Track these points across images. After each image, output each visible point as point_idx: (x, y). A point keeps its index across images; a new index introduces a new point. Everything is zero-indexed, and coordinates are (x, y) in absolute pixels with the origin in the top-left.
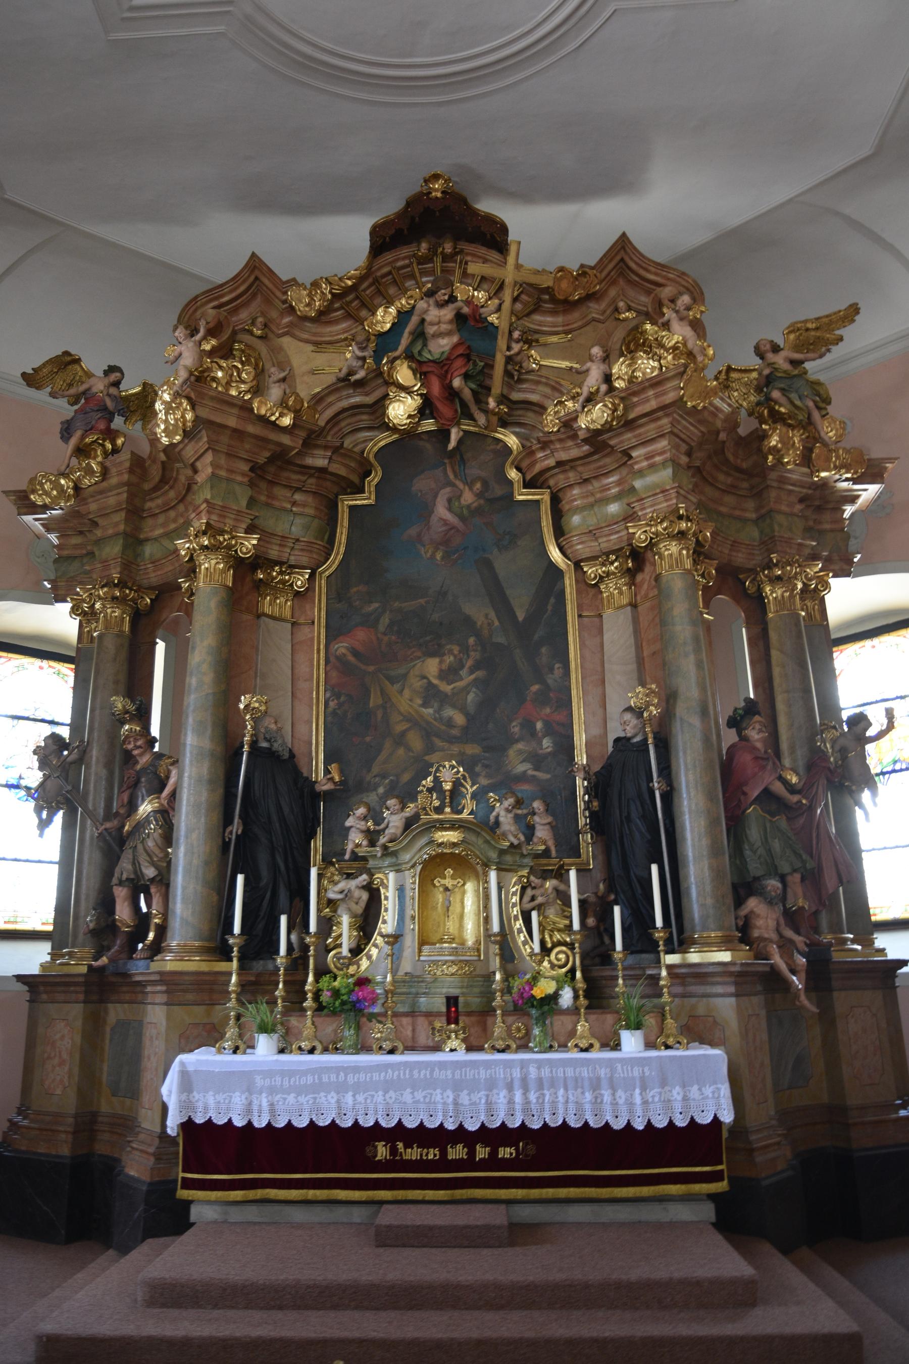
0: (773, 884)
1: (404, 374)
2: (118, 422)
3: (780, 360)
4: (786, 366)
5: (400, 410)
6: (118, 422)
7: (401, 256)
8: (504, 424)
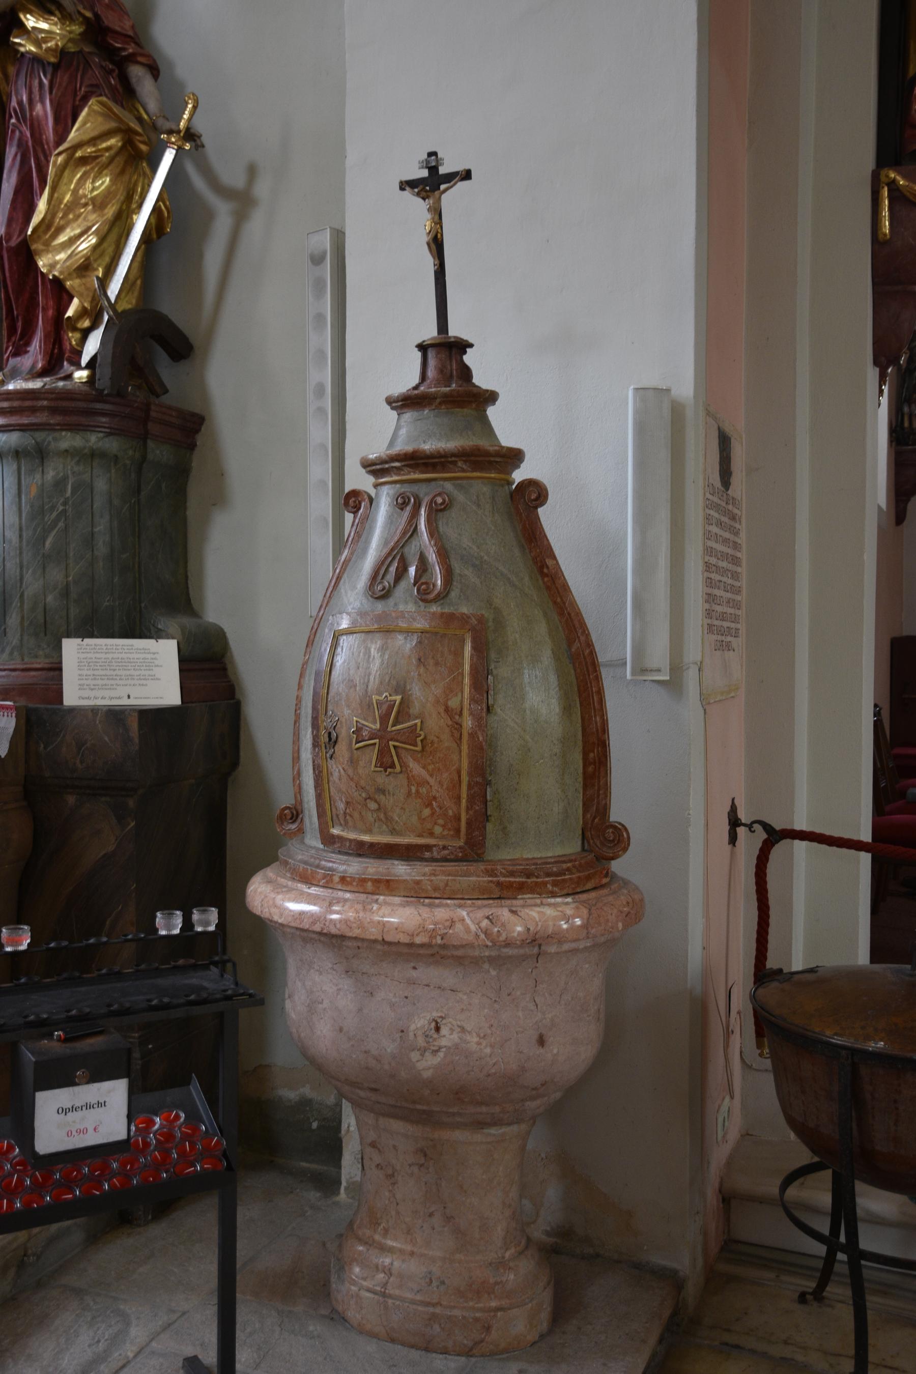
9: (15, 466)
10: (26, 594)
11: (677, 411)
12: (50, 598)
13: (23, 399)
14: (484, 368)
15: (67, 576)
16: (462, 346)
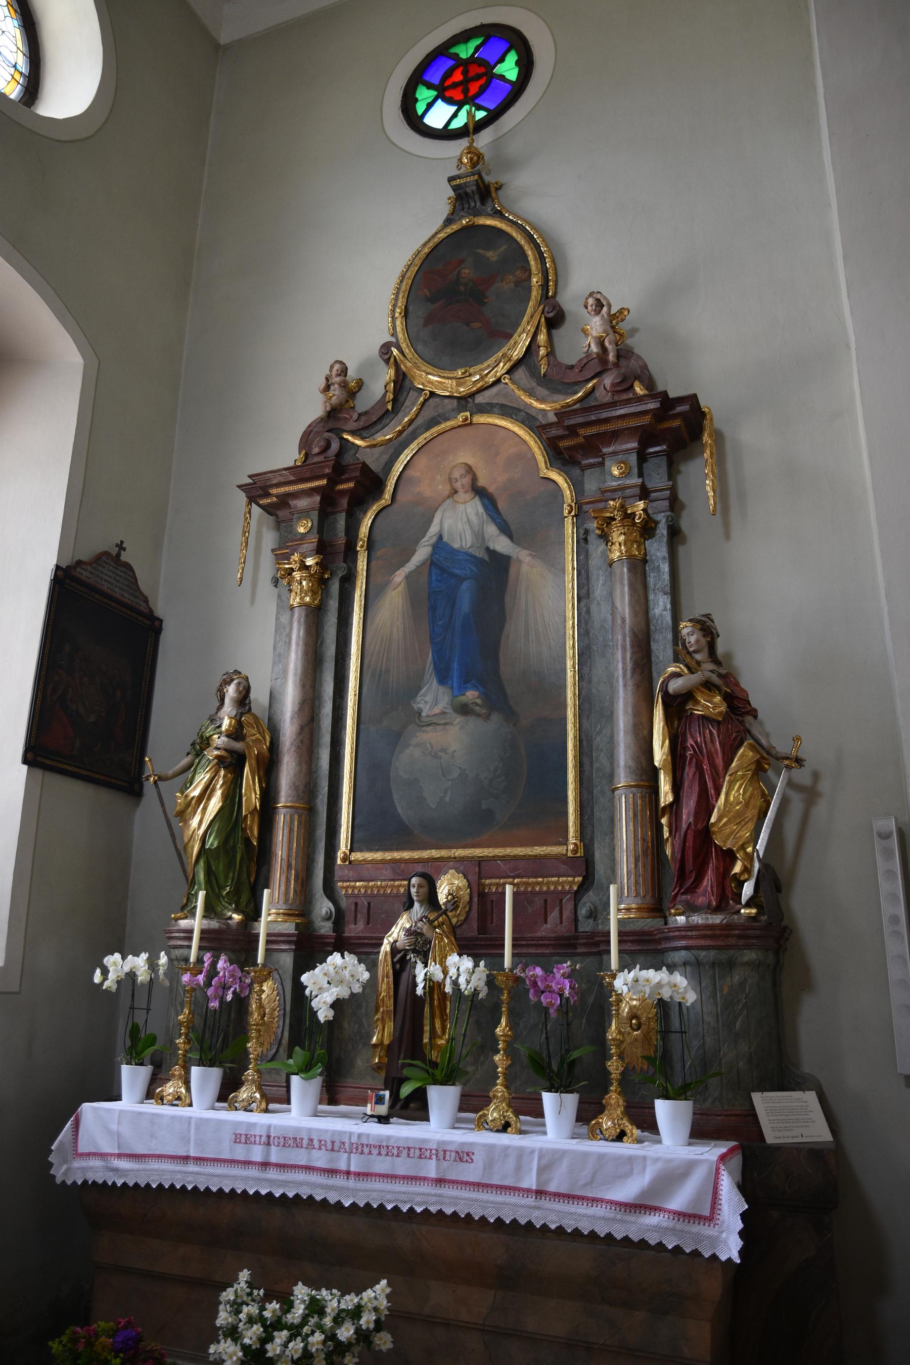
9: (711, 972)
10: (723, 1061)
12: (741, 1064)
13: (722, 930)
15: (750, 1048)
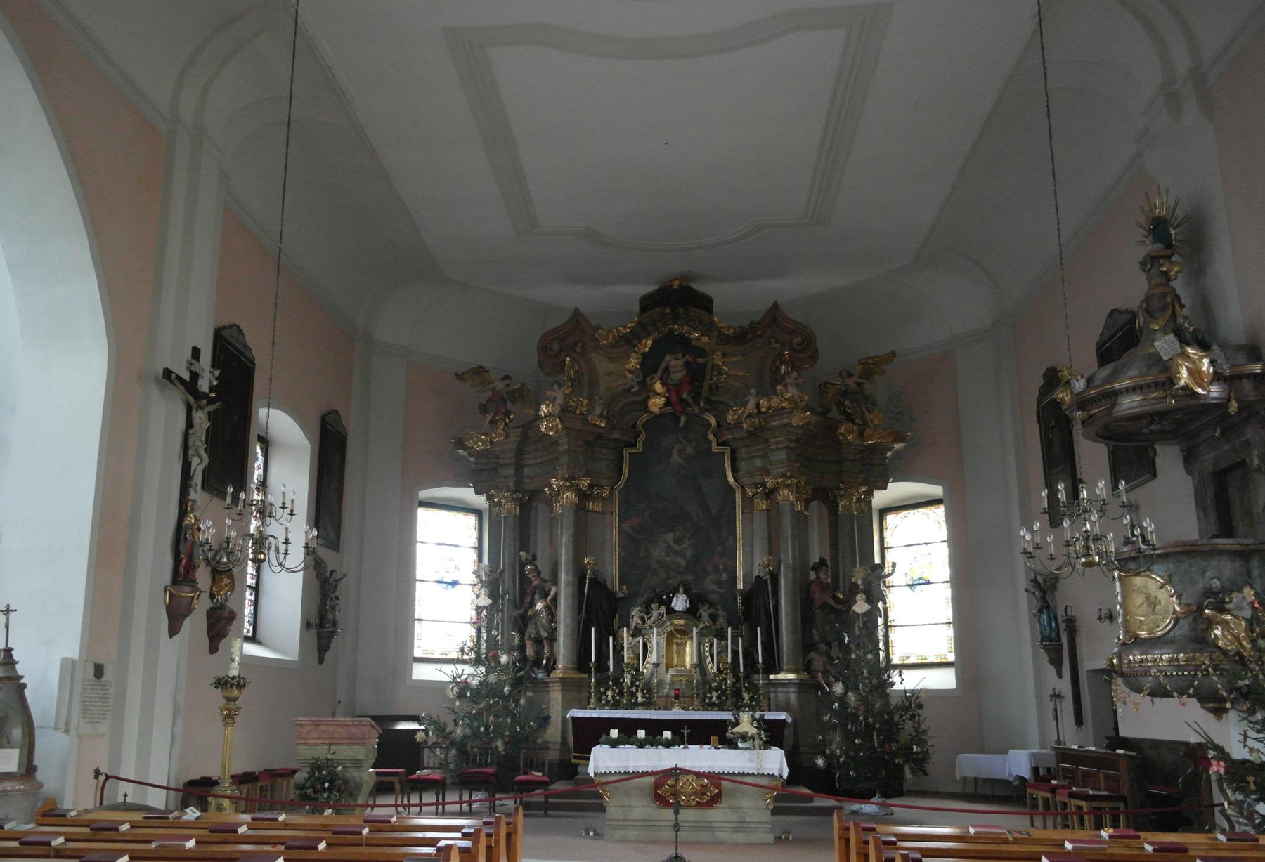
0: (823, 647)
1: (658, 387)
2: (509, 405)
3: (850, 382)
4: (854, 386)
5: (656, 404)
6: (509, 405)
7: (656, 313)
8: (707, 410)
11: (73, 662)
14: (16, 655)
16: (11, 650)
